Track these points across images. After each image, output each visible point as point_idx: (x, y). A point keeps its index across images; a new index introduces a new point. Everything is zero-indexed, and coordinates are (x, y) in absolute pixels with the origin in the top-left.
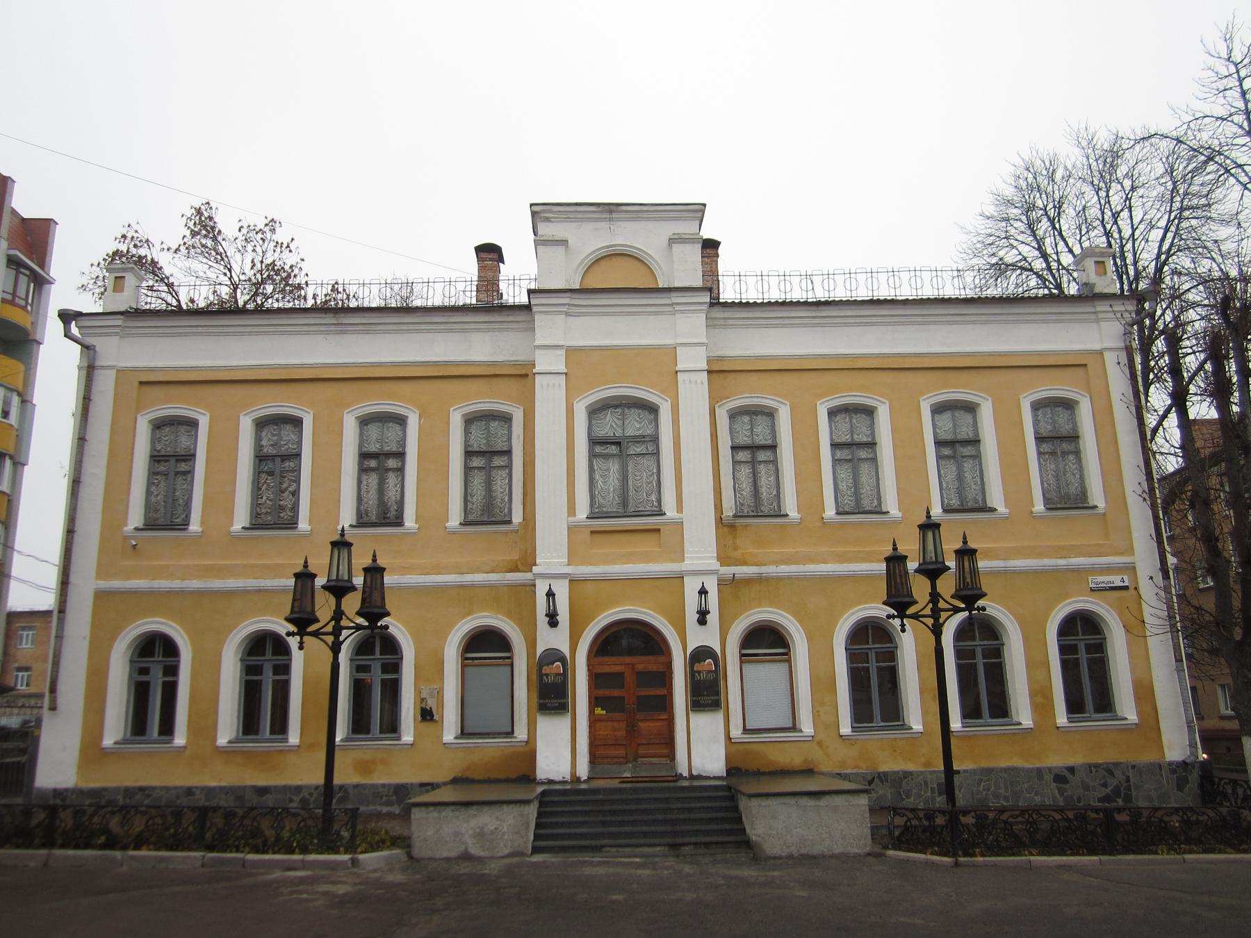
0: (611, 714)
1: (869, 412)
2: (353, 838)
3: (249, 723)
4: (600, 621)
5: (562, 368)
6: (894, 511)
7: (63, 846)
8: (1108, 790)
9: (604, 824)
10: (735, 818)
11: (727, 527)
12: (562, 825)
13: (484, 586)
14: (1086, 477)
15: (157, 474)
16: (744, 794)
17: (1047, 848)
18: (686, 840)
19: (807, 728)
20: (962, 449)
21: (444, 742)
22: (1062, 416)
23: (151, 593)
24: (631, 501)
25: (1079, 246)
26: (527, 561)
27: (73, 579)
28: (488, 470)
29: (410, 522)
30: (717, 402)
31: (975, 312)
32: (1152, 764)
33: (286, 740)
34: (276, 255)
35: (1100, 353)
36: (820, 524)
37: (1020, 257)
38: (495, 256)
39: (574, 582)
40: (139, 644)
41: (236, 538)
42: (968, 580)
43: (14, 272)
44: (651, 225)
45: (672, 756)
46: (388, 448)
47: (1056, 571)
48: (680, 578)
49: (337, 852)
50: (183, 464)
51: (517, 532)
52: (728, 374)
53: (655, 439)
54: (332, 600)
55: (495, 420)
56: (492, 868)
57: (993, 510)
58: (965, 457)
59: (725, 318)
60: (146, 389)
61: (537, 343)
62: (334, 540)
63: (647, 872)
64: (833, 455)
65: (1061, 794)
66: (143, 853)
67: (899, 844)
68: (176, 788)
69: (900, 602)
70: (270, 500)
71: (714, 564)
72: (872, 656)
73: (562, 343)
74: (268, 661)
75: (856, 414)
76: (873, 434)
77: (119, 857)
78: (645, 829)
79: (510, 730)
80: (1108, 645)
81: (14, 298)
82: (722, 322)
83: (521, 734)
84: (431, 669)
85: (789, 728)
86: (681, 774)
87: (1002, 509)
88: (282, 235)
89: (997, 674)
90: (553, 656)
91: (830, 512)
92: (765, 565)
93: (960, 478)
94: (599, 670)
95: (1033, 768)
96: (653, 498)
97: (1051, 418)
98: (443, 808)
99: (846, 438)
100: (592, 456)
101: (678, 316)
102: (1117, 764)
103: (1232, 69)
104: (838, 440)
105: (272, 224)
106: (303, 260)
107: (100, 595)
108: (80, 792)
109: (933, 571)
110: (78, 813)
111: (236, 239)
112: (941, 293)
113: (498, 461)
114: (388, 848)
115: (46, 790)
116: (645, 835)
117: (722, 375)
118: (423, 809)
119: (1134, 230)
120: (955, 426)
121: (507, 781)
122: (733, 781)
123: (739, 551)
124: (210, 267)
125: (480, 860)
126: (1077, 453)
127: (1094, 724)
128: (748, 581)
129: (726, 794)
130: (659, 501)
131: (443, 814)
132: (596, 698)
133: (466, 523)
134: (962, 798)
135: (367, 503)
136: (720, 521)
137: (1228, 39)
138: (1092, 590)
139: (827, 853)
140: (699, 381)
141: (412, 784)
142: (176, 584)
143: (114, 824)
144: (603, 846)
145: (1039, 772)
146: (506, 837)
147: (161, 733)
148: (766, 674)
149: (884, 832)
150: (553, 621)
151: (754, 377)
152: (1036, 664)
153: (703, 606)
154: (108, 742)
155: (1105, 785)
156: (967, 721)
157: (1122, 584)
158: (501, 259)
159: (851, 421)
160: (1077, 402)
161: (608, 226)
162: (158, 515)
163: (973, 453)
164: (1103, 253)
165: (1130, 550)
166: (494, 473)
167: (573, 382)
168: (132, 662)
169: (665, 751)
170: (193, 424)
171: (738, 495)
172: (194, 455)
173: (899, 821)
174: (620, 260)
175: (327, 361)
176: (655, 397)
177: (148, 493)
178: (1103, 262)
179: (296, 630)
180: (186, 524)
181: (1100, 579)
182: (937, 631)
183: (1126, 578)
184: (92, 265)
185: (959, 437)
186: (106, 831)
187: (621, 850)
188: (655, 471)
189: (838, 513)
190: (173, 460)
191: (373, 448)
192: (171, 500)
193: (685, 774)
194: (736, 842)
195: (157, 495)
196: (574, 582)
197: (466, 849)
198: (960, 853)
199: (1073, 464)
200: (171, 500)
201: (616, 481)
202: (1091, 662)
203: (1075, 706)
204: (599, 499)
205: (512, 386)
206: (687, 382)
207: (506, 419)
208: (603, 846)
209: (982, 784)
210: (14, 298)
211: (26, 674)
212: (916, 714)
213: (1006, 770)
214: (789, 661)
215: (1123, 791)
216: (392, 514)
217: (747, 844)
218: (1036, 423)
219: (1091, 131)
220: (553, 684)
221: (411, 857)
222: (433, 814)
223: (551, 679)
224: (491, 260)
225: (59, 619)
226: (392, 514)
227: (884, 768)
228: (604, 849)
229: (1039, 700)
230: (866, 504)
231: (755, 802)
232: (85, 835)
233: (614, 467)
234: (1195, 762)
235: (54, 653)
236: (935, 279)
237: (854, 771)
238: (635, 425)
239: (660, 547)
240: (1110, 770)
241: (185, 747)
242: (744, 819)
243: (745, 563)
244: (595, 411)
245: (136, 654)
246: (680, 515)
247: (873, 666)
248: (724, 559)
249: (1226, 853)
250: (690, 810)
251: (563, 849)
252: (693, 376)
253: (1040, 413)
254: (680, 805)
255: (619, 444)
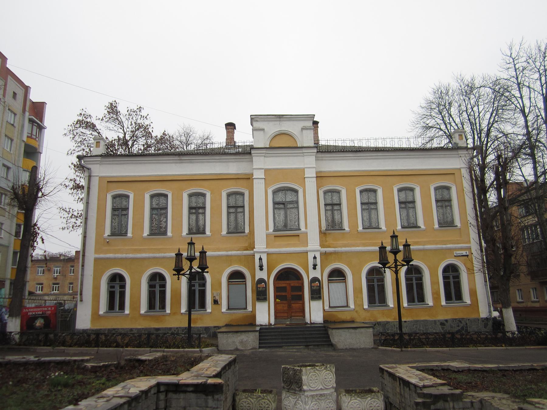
0: (282, 301)
1: (375, 191)
2: (199, 343)
3: (151, 306)
4: (278, 268)
5: (263, 177)
6: (384, 228)
7: (102, 347)
8: (459, 328)
9: (282, 339)
10: (327, 337)
11: (323, 234)
12: (268, 339)
13: (235, 256)
14: (454, 215)
15: (115, 215)
16: (330, 328)
17: (432, 346)
18: (311, 344)
19: (352, 306)
20: (408, 205)
21: (181, 312)
22: (445, 192)
23: (115, 259)
24: (288, 225)
25: (459, 118)
26: (252, 247)
27: (86, 254)
28: (236, 213)
29: (208, 232)
30: (319, 188)
31: (414, 154)
32: (476, 319)
33: (165, 311)
34: (141, 120)
35: (460, 169)
36: (357, 232)
37: (436, 123)
38: (233, 127)
39: (269, 254)
40: (110, 278)
41: (144, 238)
42: (407, 255)
43: (31, 125)
44: (295, 123)
45: (304, 316)
46: (199, 205)
47: (442, 249)
48: (307, 253)
49: (194, 348)
50: (124, 212)
51: (247, 236)
52: (323, 178)
53: (297, 202)
54: (189, 263)
55: (238, 195)
56: (247, 353)
57: (420, 227)
58: (410, 208)
59: (322, 157)
60: (110, 184)
61: (254, 167)
62: (189, 242)
63: (299, 353)
64: (362, 207)
65: (443, 329)
66: (129, 349)
67: (382, 345)
68: (126, 329)
69: (384, 262)
70: (157, 225)
71: (318, 247)
72: (375, 280)
73: (263, 167)
74: (158, 283)
75: (370, 192)
76: (376, 200)
77: (122, 350)
78: (296, 340)
79: (245, 307)
80: (461, 276)
81: (31, 135)
82: (321, 158)
83: (250, 308)
84: (217, 285)
85: (346, 306)
86: (307, 323)
87: (423, 227)
88: (144, 113)
89: (420, 287)
90: (261, 281)
91: (360, 228)
92: (337, 247)
93: (408, 215)
94: (277, 286)
95: (433, 320)
96: (297, 224)
97: (441, 193)
98: (228, 333)
99: (366, 201)
100: (274, 208)
101: (305, 157)
102: (463, 319)
103: (511, 60)
104: (363, 202)
105: (140, 108)
106: (152, 123)
107: (96, 260)
108: (90, 330)
109: (395, 252)
110: (106, 336)
111: (126, 115)
112: (402, 147)
113: (240, 210)
114: (210, 347)
115: (80, 330)
116: (297, 342)
117: (321, 178)
118: (222, 334)
119: (479, 114)
120: (406, 196)
121: (245, 325)
122: (326, 325)
123: (328, 243)
124: (115, 126)
125: (242, 350)
126: (451, 206)
127: (455, 304)
128: (331, 253)
129: (324, 329)
130: (299, 225)
131: (229, 335)
132: (277, 296)
133: (228, 233)
134: (404, 330)
135: (192, 225)
136: (320, 231)
137: (511, 49)
138: (455, 256)
139: (358, 348)
140: (313, 181)
141: (211, 327)
142: (124, 256)
143: (119, 338)
144: (282, 346)
145: (435, 322)
146: (250, 343)
147: (119, 309)
148: (337, 287)
149: (378, 341)
150: (261, 268)
151: (332, 179)
152: (434, 283)
153: (315, 263)
154: (101, 312)
155: (458, 326)
156: (410, 303)
157: (466, 254)
158: (235, 128)
159: (368, 194)
160: (451, 187)
161: (279, 123)
162: (116, 230)
163: (413, 206)
164: (462, 131)
165: (469, 242)
166: (238, 214)
167: (267, 182)
168: (108, 284)
169: (302, 314)
170: (128, 197)
171: (327, 222)
172: (128, 208)
173: (383, 338)
174: (284, 136)
175: (176, 173)
176: (297, 187)
177: (112, 222)
178: (462, 135)
179: (177, 273)
180: (126, 233)
181: (458, 252)
182: (396, 272)
183: (467, 252)
184: (68, 126)
185: (408, 200)
186: (116, 342)
187: (288, 347)
188: (297, 214)
189: (363, 229)
190: (120, 210)
191: (194, 205)
192: (120, 224)
193: (309, 322)
194: (327, 344)
195: (115, 223)
196: (269, 254)
197: (237, 347)
198: (403, 347)
199: (449, 210)
200: (120, 224)
201: (283, 218)
202: (454, 282)
203: (448, 297)
204: (277, 224)
205: (244, 182)
206: (309, 181)
207: (242, 194)
208: (282, 346)
209: (415, 326)
210: (31, 135)
211: (57, 286)
212: (391, 302)
213: (423, 321)
214: (345, 282)
215: (465, 328)
216: (201, 229)
217: (331, 345)
218: (436, 195)
219: (463, 76)
220: (262, 291)
221: (218, 350)
222: (225, 335)
223: (261, 289)
224: (231, 129)
225: (82, 268)
226: (201, 229)
227: (379, 320)
228: (283, 347)
229: (435, 296)
230: (374, 225)
231: (334, 331)
232: (109, 343)
233: (282, 212)
234: (490, 318)
235: (81, 281)
236: (399, 142)
237: (369, 321)
238: (290, 197)
239: (299, 241)
240: (460, 321)
241: (129, 314)
242: (330, 337)
243: (329, 247)
244: (275, 192)
245: (109, 281)
246: (306, 230)
247: (376, 284)
248: (322, 246)
249: (492, 347)
250: (311, 334)
251: (269, 347)
252: (310, 179)
253: (437, 191)
254: (308, 333)
255: (284, 204)
